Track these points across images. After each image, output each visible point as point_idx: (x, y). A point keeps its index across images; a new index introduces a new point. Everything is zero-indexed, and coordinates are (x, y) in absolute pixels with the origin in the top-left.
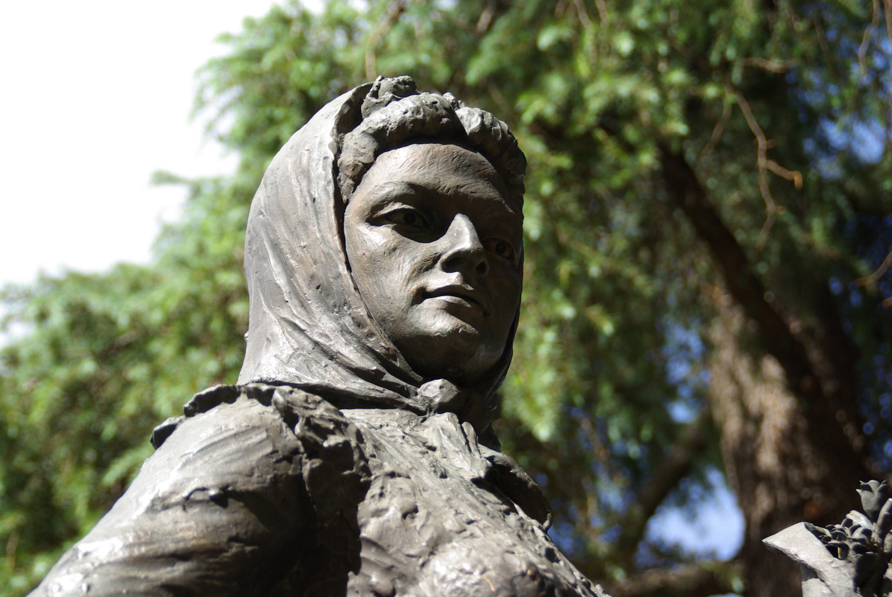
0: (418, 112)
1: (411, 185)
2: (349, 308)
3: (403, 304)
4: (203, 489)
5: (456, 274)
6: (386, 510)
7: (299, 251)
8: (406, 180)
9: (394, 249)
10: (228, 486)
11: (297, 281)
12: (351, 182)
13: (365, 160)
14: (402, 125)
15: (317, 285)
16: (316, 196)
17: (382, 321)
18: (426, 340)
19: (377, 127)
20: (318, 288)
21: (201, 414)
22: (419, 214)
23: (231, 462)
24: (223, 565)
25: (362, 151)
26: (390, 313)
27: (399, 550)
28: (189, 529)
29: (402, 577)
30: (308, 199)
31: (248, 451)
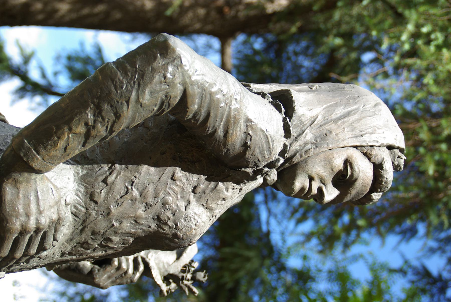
0: (385, 183)
1: (356, 180)
2: (314, 148)
3: (309, 172)
4: (251, 140)
5: (316, 192)
6: (227, 191)
7: (343, 126)
8: (359, 179)
9: (332, 170)
10: (250, 148)
11: (331, 124)
12: (365, 152)
13: (373, 159)
14: (382, 176)
15: (327, 134)
16: (364, 137)
17: (305, 161)
18: (293, 178)
19: (384, 166)
20: (326, 134)
21: (282, 125)
22: (343, 180)
23: (259, 148)
24: (219, 146)
25: (376, 158)
26: (307, 165)
27: (210, 196)
28: (236, 136)
29: (200, 197)
30: (363, 133)
31: (262, 153)
